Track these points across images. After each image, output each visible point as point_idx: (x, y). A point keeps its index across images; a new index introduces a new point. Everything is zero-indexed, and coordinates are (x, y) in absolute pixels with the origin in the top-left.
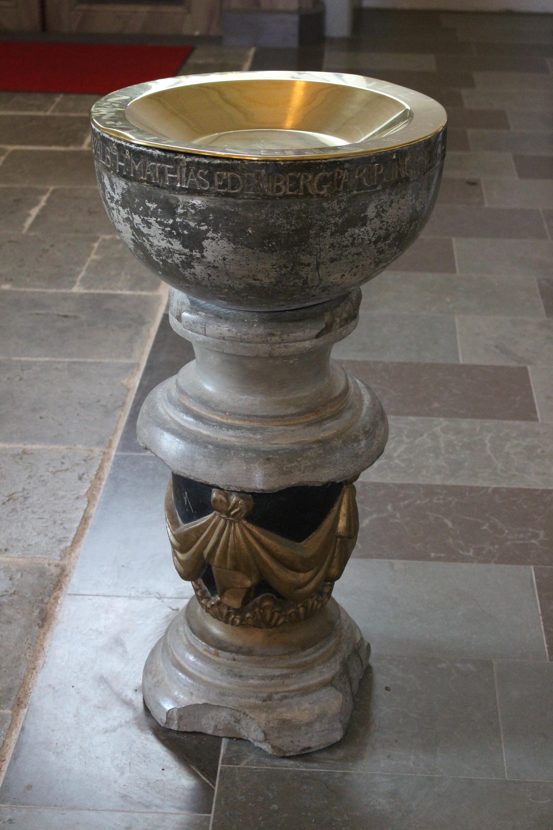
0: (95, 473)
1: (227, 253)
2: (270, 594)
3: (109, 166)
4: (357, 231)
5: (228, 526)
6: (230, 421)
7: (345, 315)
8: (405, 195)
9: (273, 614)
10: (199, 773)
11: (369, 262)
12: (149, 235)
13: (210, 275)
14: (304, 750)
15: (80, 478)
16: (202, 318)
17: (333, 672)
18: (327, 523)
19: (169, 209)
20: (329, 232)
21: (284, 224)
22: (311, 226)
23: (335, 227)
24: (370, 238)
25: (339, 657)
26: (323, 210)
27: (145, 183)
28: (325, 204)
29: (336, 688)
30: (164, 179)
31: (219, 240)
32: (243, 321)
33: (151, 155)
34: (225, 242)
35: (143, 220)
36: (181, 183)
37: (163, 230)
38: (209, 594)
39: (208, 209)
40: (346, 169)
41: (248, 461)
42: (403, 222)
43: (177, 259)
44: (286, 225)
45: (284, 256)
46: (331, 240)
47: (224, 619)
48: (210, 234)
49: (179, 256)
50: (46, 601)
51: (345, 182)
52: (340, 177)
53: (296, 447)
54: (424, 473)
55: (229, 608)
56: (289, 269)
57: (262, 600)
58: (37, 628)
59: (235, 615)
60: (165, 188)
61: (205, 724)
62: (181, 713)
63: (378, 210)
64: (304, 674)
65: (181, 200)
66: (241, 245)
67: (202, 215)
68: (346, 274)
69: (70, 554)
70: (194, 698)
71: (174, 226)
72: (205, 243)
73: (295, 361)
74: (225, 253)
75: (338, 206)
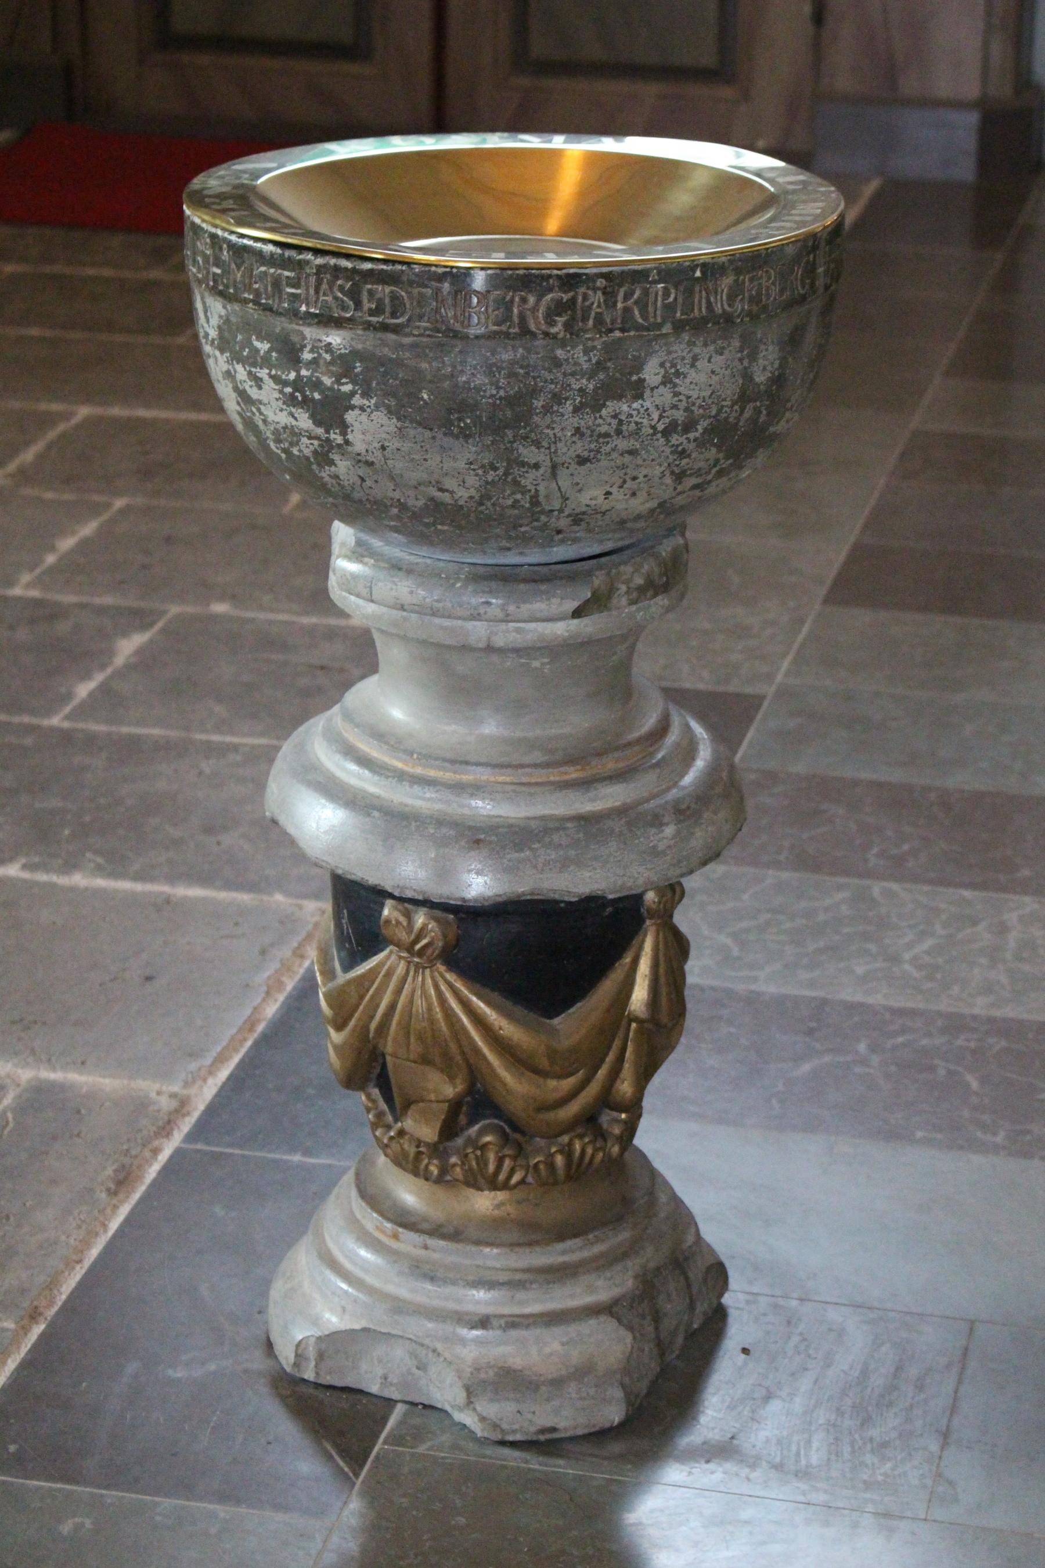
0: (295, 945)
1: (388, 437)
2: (496, 1121)
3: (200, 276)
4: (625, 408)
5: (412, 973)
6: (419, 771)
7: (639, 581)
8: (724, 348)
9: (500, 1161)
10: (334, 1453)
11: (658, 471)
12: (260, 402)
13: (363, 480)
14: (543, 1431)
15: (263, 952)
16: (367, 569)
17: (617, 1292)
18: (608, 986)
19: (290, 352)
20: (568, 407)
21: (484, 385)
22: (534, 392)
23: (581, 397)
24: (653, 423)
25: (634, 1265)
26: (557, 363)
27: (251, 305)
28: (560, 353)
29: (619, 1320)
30: (280, 298)
31: (372, 412)
32: (439, 575)
33: (260, 254)
34: (383, 416)
35: (250, 373)
36: (307, 305)
37: (281, 392)
38: (389, 1118)
39: (355, 354)
40: (599, 289)
41: (442, 843)
42: (725, 400)
43: (306, 447)
44: (488, 387)
45: (488, 446)
46: (575, 421)
47: (410, 1166)
48: (357, 400)
49: (309, 442)
50: (133, 1153)
51: (597, 313)
52: (587, 303)
53: (533, 824)
54: (956, 989)
55: (419, 1143)
56: (500, 472)
57: (481, 1133)
58: (104, 1195)
59: (430, 1158)
60: (281, 314)
61: (366, 1372)
62: (323, 1346)
63: (666, 372)
64: (556, 1286)
65: (308, 336)
66: (411, 422)
67: (344, 365)
68: (614, 490)
69: (205, 1080)
70: (347, 1317)
71: (298, 384)
72: (350, 416)
73: (543, 664)
74: (384, 436)
75: (586, 358)
